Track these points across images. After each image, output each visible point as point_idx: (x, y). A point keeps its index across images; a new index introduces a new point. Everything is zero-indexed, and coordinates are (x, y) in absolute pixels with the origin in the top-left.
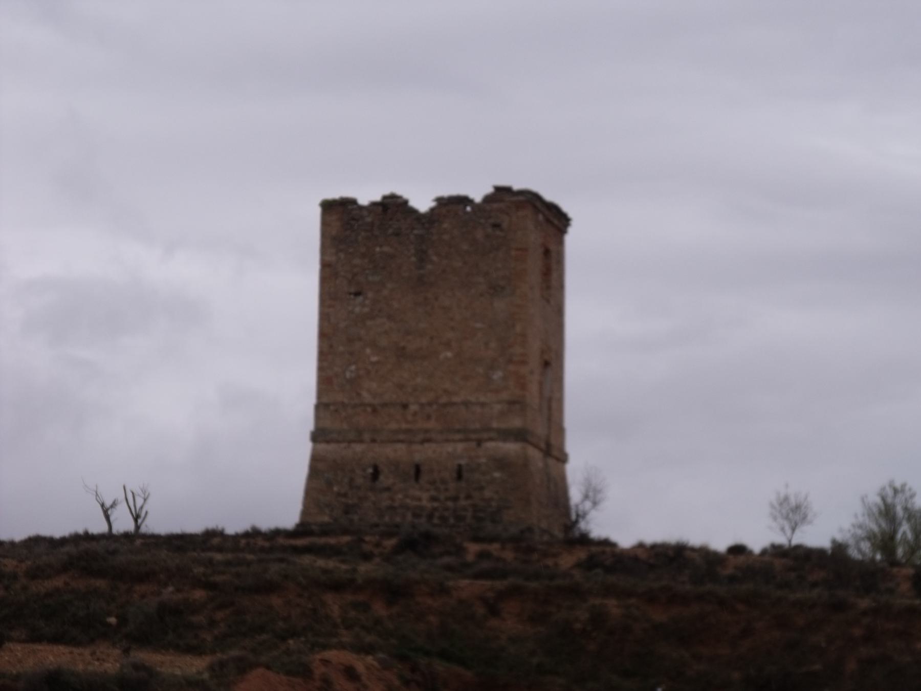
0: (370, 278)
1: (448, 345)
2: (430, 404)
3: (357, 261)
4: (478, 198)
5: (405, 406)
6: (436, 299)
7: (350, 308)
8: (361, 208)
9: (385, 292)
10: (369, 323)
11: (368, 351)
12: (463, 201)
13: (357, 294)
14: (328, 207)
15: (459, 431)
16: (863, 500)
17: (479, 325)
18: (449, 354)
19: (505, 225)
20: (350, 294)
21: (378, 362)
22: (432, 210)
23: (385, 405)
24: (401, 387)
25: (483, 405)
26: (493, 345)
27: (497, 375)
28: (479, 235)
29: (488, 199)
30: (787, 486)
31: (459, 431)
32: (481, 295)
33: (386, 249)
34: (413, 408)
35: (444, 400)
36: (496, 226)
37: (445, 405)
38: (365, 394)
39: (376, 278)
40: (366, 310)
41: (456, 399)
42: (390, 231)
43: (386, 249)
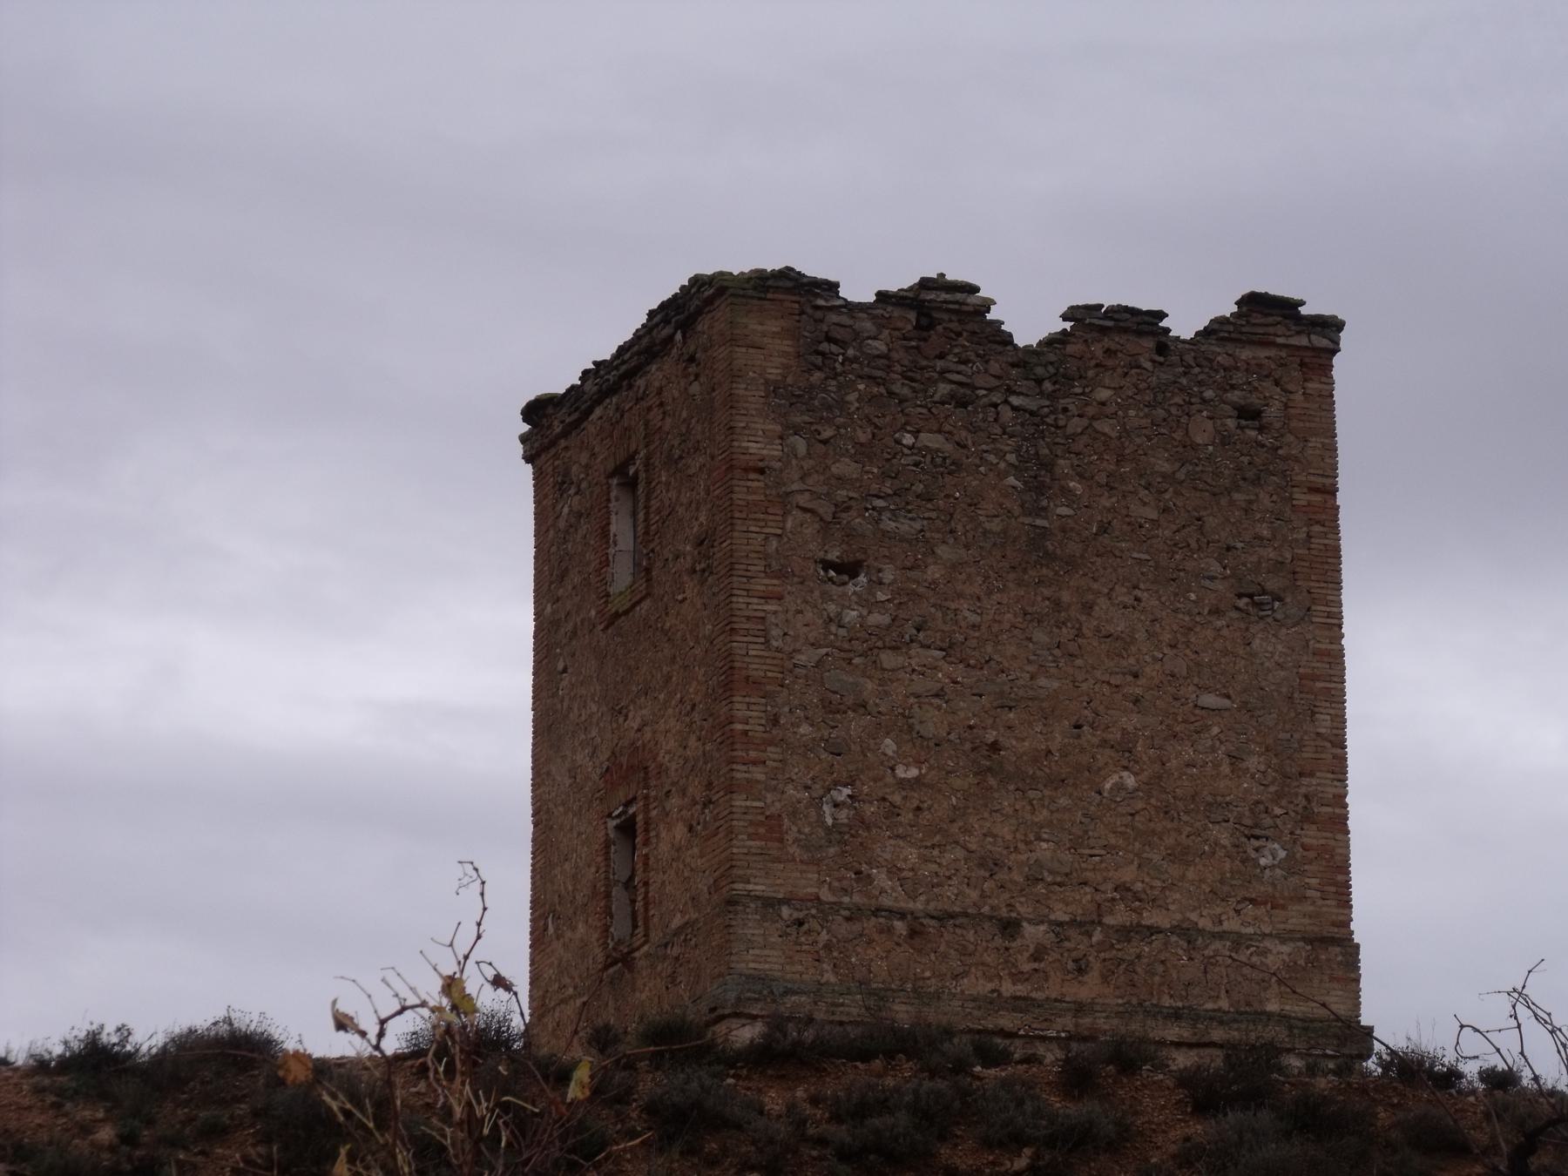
0: (889, 525)
1: (1125, 749)
2: (1084, 926)
3: (845, 467)
4: (1184, 324)
5: (1010, 927)
6: (1088, 608)
7: (832, 608)
8: (853, 308)
9: (934, 572)
10: (888, 659)
11: (889, 746)
12: (1147, 323)
13: (849, 569)
14: (1330, 327)
15: (1176, 1015)
16: (31, 1044)
17: (1209, 700)
18: (1130, 781)
19: (1272, 412)
20: (827, 565)
21: (917, 782)
22: (1051, 342)
23: (944, 917)
24: (991, 865)
25: (1238, 941)
26: (1253, 763)
27: (1272, 854)
28: (1202, 431)
29: (1215, 330)
30: (92, 1024)
31: (1176, 1015)
32: (1216, 612)
33: (929, 440)
34: (1034, 933)
35: (1120, 916)
36: (1249, 414)
37: (1126, 933)
38: (881, 879)
39: (905, 527)
40: (877, 619)
41: (1151, 918)
42: (944, 389)
43: (929, 440)
